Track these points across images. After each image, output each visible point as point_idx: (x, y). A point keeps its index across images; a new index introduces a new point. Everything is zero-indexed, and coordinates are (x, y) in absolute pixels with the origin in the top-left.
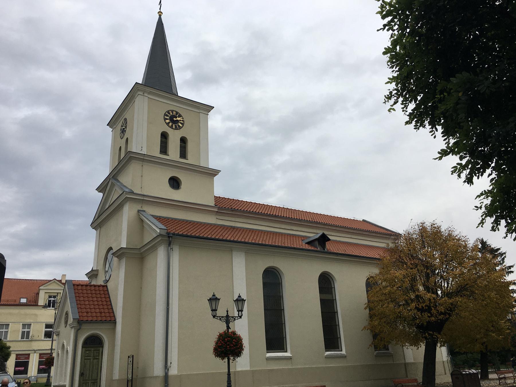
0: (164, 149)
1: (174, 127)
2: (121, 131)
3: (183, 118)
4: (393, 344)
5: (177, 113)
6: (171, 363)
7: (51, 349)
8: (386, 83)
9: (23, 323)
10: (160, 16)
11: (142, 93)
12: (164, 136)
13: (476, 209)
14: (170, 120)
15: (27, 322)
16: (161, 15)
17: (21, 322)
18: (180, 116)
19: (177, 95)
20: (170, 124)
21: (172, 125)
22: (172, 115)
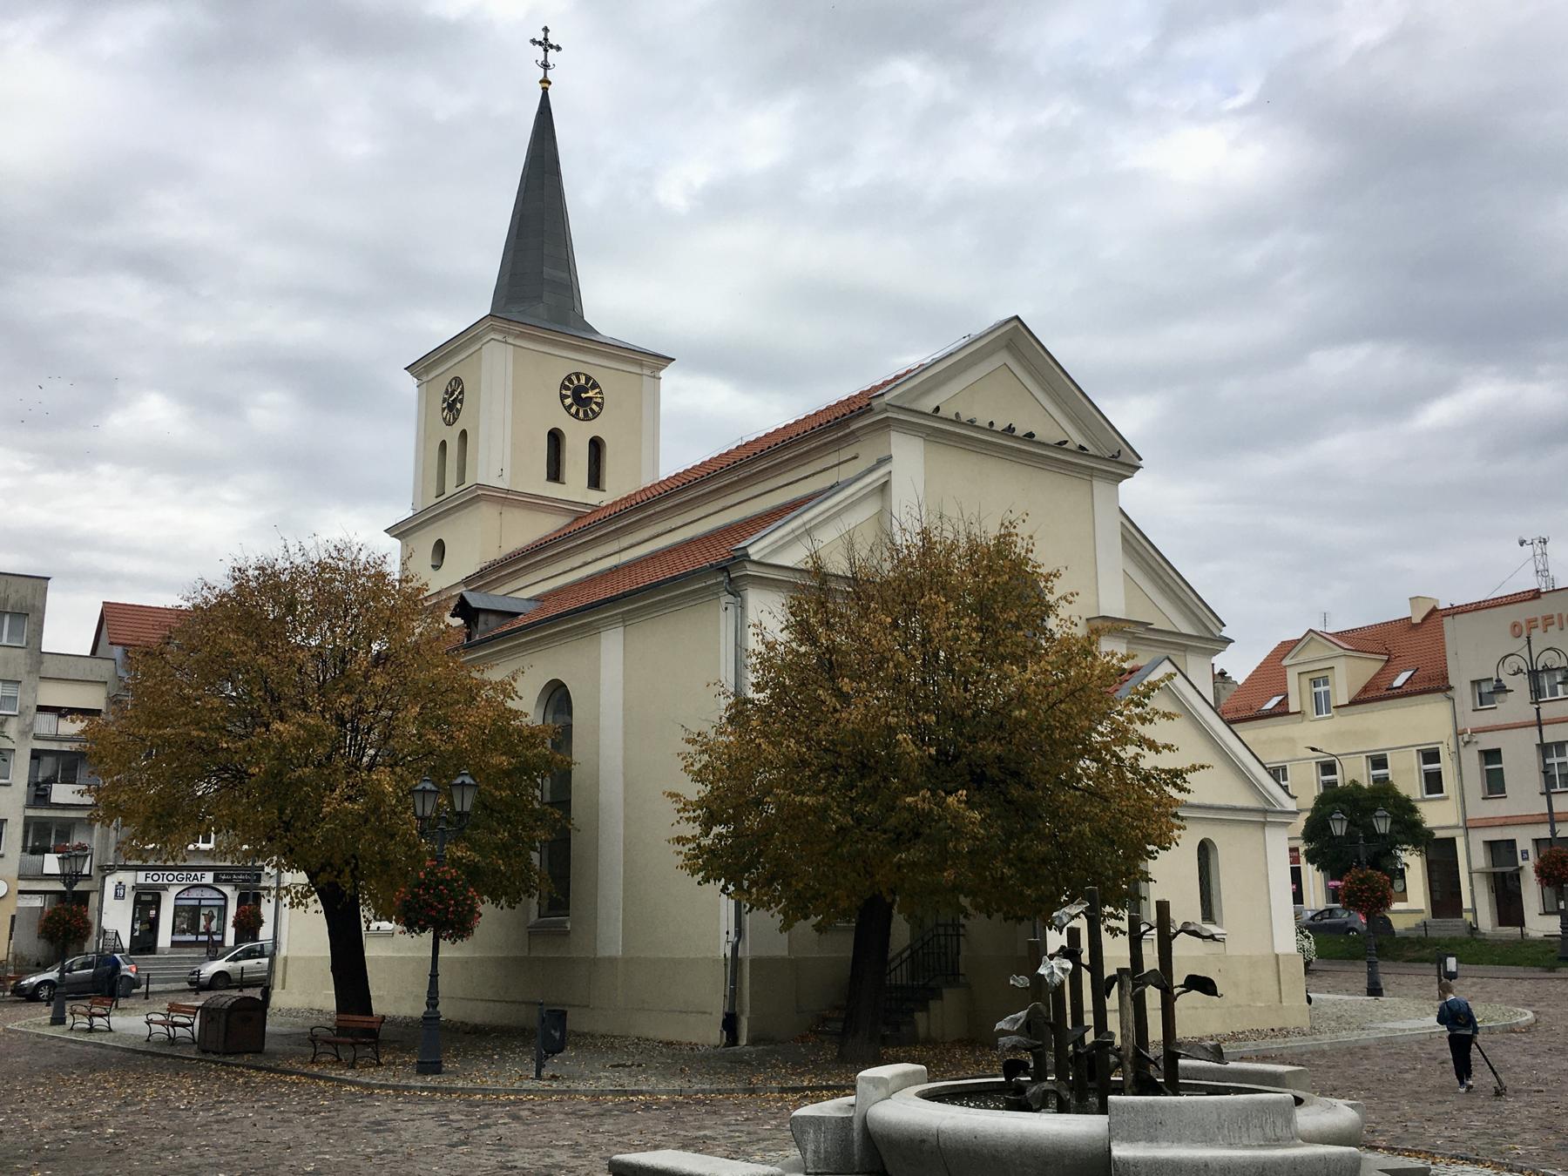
1: (581, 414)
2: (445, 405)
3: (600, 393)
5: (588, 378)
6: (1313, 749)
9: (1419, 748)
10: (545, 90)
11: (499, 337)
12: (555, 438)
13: (79, 792)
14: (573, 393)
15: (1221, 738)
16: (547, 89)
17: (1362, 753)
18: (595, 386)
21: (571, 406)
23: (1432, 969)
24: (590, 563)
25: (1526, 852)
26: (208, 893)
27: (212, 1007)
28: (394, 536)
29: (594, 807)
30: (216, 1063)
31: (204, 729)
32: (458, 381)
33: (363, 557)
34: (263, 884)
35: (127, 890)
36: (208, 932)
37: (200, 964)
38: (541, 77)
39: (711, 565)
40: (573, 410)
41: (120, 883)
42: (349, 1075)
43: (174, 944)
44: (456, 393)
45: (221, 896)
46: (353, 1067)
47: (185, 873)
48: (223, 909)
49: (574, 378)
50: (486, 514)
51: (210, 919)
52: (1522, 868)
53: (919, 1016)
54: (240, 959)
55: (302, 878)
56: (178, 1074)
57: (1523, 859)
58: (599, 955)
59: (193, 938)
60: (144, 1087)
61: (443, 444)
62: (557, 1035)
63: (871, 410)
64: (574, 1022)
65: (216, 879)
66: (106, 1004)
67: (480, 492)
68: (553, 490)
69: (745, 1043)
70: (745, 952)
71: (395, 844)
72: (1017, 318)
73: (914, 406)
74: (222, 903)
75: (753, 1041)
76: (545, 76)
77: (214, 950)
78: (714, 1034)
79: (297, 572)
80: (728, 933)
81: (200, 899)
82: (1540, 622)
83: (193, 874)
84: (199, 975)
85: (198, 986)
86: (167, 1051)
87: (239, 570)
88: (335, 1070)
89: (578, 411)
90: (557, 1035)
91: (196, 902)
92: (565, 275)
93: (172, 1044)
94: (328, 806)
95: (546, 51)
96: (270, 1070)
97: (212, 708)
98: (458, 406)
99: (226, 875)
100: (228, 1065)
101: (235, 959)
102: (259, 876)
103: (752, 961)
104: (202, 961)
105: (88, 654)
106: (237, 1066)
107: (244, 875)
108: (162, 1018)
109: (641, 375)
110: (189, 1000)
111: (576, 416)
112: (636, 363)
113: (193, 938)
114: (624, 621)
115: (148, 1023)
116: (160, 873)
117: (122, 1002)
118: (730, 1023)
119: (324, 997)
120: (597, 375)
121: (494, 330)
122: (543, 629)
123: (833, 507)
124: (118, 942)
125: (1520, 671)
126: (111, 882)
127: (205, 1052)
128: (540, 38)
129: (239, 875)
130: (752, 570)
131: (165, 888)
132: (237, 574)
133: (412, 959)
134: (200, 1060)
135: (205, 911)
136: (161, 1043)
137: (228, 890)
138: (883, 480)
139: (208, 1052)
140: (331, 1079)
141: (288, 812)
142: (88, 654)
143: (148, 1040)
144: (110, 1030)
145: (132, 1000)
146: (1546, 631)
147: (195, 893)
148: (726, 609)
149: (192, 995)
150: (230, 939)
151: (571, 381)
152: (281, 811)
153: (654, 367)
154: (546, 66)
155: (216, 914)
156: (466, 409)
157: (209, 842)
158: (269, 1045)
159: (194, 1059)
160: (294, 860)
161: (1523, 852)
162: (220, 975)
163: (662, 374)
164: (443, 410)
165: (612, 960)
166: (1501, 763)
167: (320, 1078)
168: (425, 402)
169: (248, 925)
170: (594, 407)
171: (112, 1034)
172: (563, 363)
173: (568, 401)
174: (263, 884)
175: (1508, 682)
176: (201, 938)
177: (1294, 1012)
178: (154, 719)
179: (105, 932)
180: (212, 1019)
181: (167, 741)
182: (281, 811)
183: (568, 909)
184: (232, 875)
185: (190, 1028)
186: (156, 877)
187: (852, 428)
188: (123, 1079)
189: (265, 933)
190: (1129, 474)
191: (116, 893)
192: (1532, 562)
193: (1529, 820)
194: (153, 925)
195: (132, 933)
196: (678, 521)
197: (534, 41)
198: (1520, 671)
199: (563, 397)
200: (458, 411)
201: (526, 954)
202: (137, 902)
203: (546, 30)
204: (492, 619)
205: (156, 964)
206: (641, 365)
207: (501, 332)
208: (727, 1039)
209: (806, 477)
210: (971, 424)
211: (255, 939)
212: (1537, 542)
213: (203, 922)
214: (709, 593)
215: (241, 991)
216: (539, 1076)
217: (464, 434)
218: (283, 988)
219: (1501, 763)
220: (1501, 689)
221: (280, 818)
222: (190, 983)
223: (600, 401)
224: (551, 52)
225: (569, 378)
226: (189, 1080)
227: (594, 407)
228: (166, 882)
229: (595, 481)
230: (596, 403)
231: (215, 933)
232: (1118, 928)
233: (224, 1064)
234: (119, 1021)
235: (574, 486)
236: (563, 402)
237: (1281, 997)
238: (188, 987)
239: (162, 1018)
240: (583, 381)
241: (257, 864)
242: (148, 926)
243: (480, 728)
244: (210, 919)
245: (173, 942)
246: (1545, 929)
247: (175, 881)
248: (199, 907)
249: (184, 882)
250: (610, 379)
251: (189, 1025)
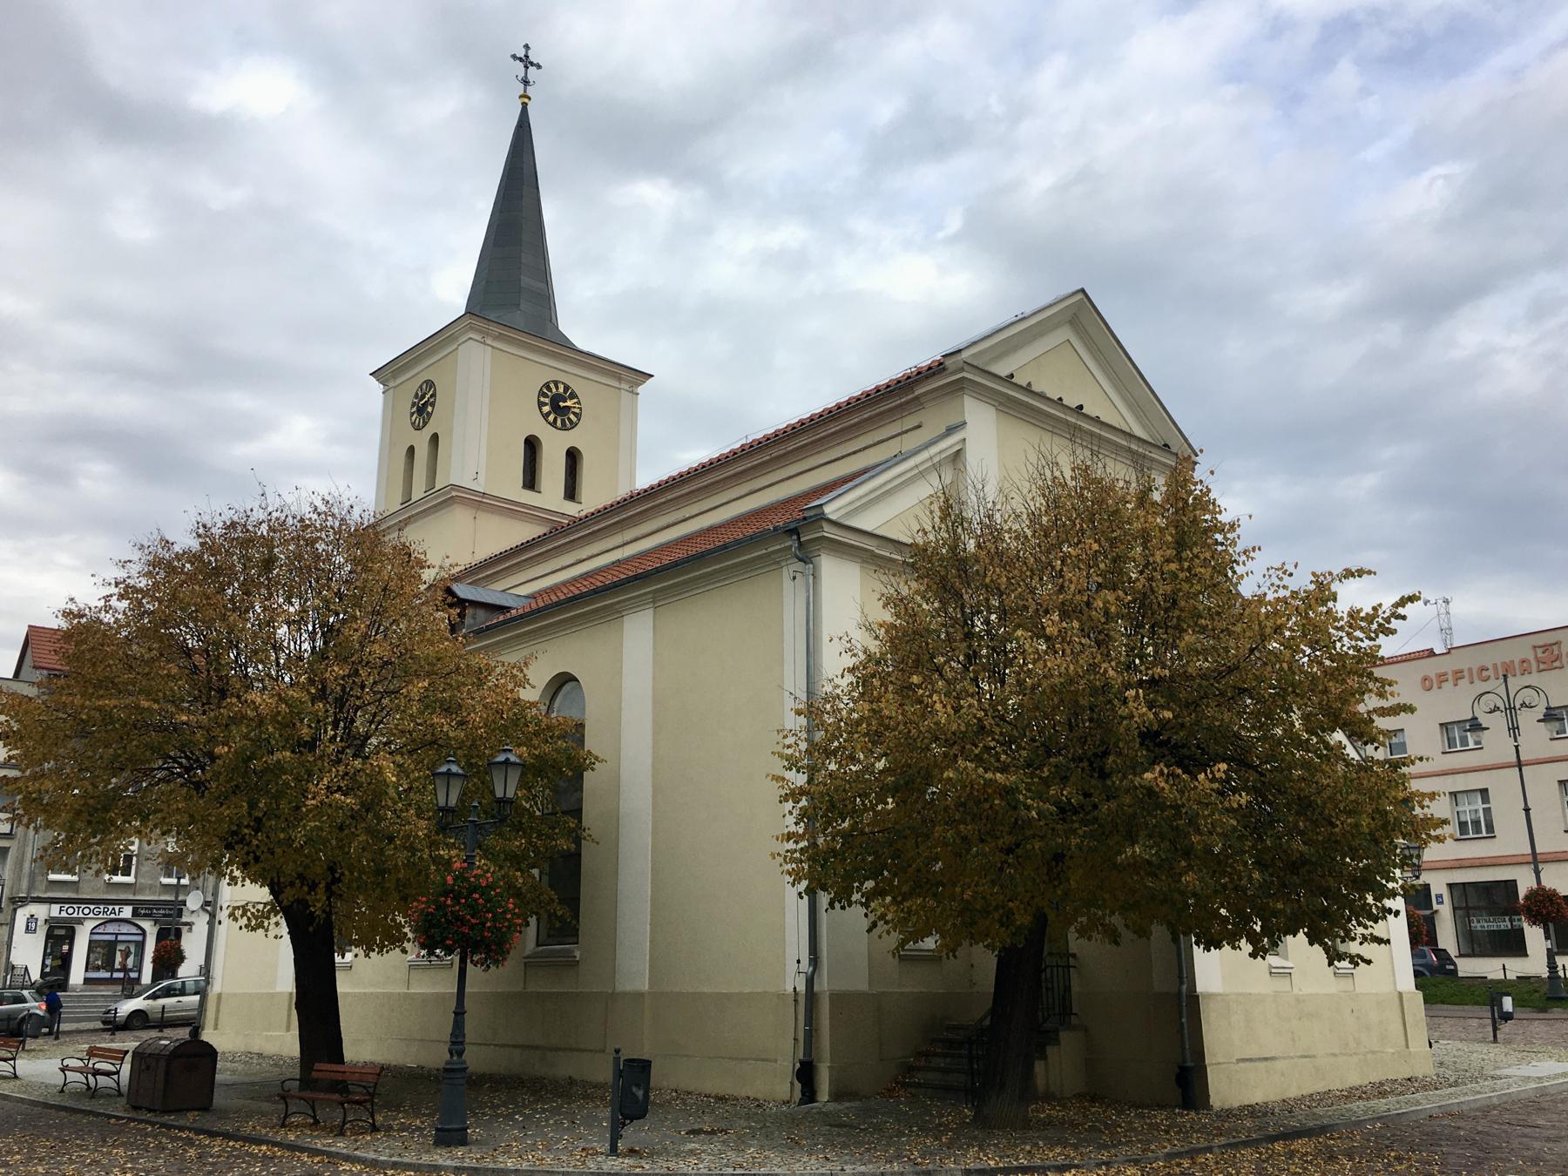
0: (531, 481)
2: (414, 409)
3: (579, 403)
4: (232, 915)
5: (567, 388)
8: (1539, 721)
10: (525, 105)
12: (532, 446)
18: (573, 396)
21: (548, 414)
22: (560, 395)
23: (1485, 1012)
24: (584, 560)
25: (1441, 896)
26: (125, 928)
27: (148, 1051)
29: (614, 819)
30: (153, 1124)
31: (156, 701)
32: (430, 384)
33: (356, 513)
34: (184, 919)
35: (39, 923)
36: (124, 969)
37: (116, 1002)
38: (522, 92)
39: (776, 529)
40: (551, 418)
41: (32, 916)
42: (341, 1146)
43: (87, 981)
44: (427, 396)
45: (139, 932)
46: (341, 1133)
47: (102, 907)
48: (141, 946)
49: (552, 385)
50: (460, 517)
51: (126, 954)
52: (1436, 911)
53: (1039, 1067)
54: (159, 997)
55: (259, 894)
56: (104, 1141)
57: (1438, 903)
58: (620, 988)
59: (107, 975)
60: (60, 1163)
61: (411, 450)
62: (640, 1093)
63: (944, 369)
64: (660, 1076)
65: (135, 913)
66: (10, 1047)
67: (454, 494)
68: (528, 497)
69: (826, 1098)
70: (823, 985)
71: (395, 848)
72: (1083, 291)
73: (987, 368)
74: (139, 938)
75: (836, 1096)
76: (525, 91)
77: (130, 987)
78: (779, 1084)
79: (278, 527)
80: (799, 962)
81: (117, 934)
82: (1450, 677)
83: (111, 907)
84: (116, 1013)
85: (114, 1026)
86: (86, 1105)
87: (204, 526)
88: (317, 1137)
89: (555, 419)
90: (640, 1093)
91: (112, 938)
92: (542, 286)
93: (93, 1097)
94: (314, 798)
95: (526, 67)
96: (228, 1136)
97: (168, 675)
98: (430, 409)
99: (146, 909)
100: (169, 1127)
101: (154, 997)
102: (181, 911)
103: (831, 996)
104: (116, 999)
105: (11, 677)
106: (181, 1129)
107: (165, 909)
108: (80, 1064)
110: (105, 1040)
111: (553, 424)
112: (615, 377)
113: (107, 975)
114: (654, 602)
115: (63, 1070)
116: (75, 906)
117: (31, 1044)
118: (806, 1074)
119: (284, 1041)
120: (575, 386)
121: (472, 328)
122: (552, 615)
124: (27, 977)
125: (1496, 709)
126: (22, 915)
127: (136, 1108)
128: (521, 54)
129: (159, 909)
130: (829, 532)
131: (80, 921)
132: (201, 531)
133: (377, 996)
134: (133, 1120)
135: (121, 947)
136: (76, 1095)
137: (147, 925)
139: (141, 1108)
140: (316, 1152)
141: (261, 805)
142: (11, 677)
143: (62, 1091)
144: (16, 1077)
145: (40, 1041)
146: (1456, 685)
147: (111, 928)
148: (794, 578)
149: (107, 1036)
150: (147, 977)
151: (549, 389)
152: (253, 805)
153: (632, 382)
154: (526, 82)
155: (132, 950)
156: (438, 413)
157: (129, 875)
158: (219, 1099)
159: (123, 1118)
160: (255, 869)
161: (1437, 896)
162: (137, 1013)
163: (640, 389)
164: (412, 414)
165: (639, 996)
166: (1489, 803)
167: (302, 1150)
168: (390, 409)
169: (169, 960)
170: (572, 417)
171: (18, 1082)
172: (541, 371)
173: (546, 409)
174: (184, 919)
175: (1484, 720)
176: (116, 975)
177: (1421, 1062)
178: (91, 691)
179: (13, 967)
180: (148, 1068)
181: (107, 717)
182: (253, 805)
183: (577, 935)
184: (151, 909)
185: (115, 1077)
186: (70, 911)
187: (916, 393)
188: (32, 1150)
189: (188, 970)
191: (28, 926)
192: (1437, 620)
193: (1477, 863)
194: (65, 962)
195: (42, 970)
196: (694, 509)
197: (514, 57)
198: (1496, 709)
199: (541, 404)
200: (430, 415)
201: (520, 989)
202: (49, 936)
203: (527, 47)
204: (481, 613)
205: (79, 1002)
206: (620, 379)
207: (480, 332)
208: (803, 1094)
209: (855, 453)
210: (1042, 396)
211: (174, 976)
212: (1441, 602)
213: (118, 958)
214: (772, 563)
215: (161, 1031)
216: (614, 1150)
217: (435, 438)
218: (216, 1029)
219: (1489, 803)
220: (1475, 726)
221: (250, 814)
222: (104, 1023)
223: (577, 411)
224: (532, 69)
225: (547, 386)
226: (121, 1151)
227: (572, 417)
228: (81, 915)
229: (571, 493)
230: (574, 413)
231: (131, 970)
232: (1359, 956)
233: (163, 1125)
234: (25, 1066)
235: (551, 494)
236: (540, 410)
237: (1407, 1040)
238: (102, 1026)
239: (80, 1064)
240: (561, 390)
241: (180, 898)
242: (59, 962)
243: (498, 712)
244: (126, 954)
245: (85, 979)
246: (1519, 970)
247: (91, 915)
248: (116, 942)
249: (101, 916)
250: (589, 392)
251: (114, 1073)
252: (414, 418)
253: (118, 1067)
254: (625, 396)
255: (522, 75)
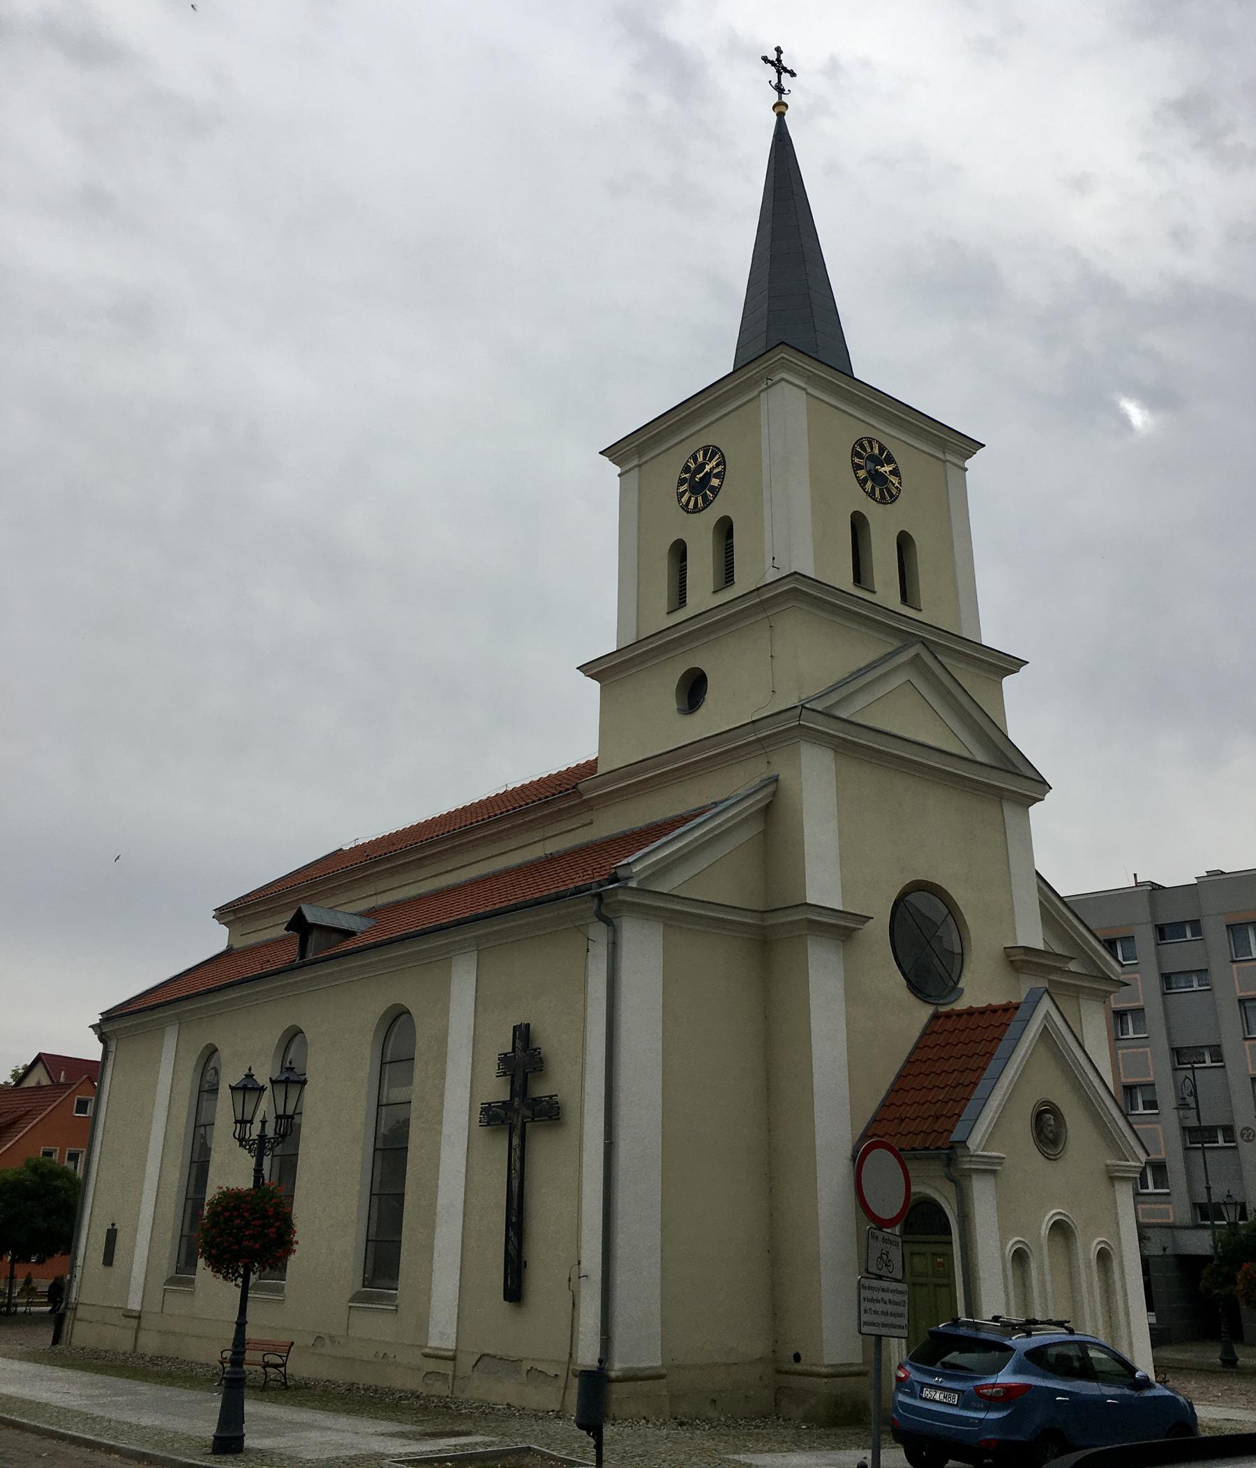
7: (456, 1350)
10: (781, 115)
12: (858, 524)
16: (784, 114)
18: (890, 460)
19: (851, 375)
20: (869, 485)
28: (591, 676)
38: (776, 100)
49: (866, 443)
61: (679, 552)
98: (715, 482)
109: (944, 461)
120: (893, 448)
123: (700, 824)
138: (767, 801)
154: (780, 89)
185: (282, 1369)
190: (1040, 797)
191: (363, 1283)
197: (765, 59)
203: (779, 50)
217: (725, 529)
251: (280, 1366)
252: (684, 500)
253: (284, 1358)
254: (952, 471)
255: (775, 82)
